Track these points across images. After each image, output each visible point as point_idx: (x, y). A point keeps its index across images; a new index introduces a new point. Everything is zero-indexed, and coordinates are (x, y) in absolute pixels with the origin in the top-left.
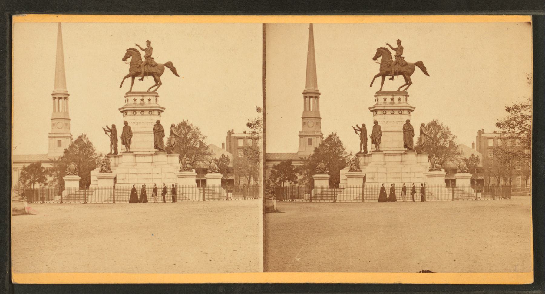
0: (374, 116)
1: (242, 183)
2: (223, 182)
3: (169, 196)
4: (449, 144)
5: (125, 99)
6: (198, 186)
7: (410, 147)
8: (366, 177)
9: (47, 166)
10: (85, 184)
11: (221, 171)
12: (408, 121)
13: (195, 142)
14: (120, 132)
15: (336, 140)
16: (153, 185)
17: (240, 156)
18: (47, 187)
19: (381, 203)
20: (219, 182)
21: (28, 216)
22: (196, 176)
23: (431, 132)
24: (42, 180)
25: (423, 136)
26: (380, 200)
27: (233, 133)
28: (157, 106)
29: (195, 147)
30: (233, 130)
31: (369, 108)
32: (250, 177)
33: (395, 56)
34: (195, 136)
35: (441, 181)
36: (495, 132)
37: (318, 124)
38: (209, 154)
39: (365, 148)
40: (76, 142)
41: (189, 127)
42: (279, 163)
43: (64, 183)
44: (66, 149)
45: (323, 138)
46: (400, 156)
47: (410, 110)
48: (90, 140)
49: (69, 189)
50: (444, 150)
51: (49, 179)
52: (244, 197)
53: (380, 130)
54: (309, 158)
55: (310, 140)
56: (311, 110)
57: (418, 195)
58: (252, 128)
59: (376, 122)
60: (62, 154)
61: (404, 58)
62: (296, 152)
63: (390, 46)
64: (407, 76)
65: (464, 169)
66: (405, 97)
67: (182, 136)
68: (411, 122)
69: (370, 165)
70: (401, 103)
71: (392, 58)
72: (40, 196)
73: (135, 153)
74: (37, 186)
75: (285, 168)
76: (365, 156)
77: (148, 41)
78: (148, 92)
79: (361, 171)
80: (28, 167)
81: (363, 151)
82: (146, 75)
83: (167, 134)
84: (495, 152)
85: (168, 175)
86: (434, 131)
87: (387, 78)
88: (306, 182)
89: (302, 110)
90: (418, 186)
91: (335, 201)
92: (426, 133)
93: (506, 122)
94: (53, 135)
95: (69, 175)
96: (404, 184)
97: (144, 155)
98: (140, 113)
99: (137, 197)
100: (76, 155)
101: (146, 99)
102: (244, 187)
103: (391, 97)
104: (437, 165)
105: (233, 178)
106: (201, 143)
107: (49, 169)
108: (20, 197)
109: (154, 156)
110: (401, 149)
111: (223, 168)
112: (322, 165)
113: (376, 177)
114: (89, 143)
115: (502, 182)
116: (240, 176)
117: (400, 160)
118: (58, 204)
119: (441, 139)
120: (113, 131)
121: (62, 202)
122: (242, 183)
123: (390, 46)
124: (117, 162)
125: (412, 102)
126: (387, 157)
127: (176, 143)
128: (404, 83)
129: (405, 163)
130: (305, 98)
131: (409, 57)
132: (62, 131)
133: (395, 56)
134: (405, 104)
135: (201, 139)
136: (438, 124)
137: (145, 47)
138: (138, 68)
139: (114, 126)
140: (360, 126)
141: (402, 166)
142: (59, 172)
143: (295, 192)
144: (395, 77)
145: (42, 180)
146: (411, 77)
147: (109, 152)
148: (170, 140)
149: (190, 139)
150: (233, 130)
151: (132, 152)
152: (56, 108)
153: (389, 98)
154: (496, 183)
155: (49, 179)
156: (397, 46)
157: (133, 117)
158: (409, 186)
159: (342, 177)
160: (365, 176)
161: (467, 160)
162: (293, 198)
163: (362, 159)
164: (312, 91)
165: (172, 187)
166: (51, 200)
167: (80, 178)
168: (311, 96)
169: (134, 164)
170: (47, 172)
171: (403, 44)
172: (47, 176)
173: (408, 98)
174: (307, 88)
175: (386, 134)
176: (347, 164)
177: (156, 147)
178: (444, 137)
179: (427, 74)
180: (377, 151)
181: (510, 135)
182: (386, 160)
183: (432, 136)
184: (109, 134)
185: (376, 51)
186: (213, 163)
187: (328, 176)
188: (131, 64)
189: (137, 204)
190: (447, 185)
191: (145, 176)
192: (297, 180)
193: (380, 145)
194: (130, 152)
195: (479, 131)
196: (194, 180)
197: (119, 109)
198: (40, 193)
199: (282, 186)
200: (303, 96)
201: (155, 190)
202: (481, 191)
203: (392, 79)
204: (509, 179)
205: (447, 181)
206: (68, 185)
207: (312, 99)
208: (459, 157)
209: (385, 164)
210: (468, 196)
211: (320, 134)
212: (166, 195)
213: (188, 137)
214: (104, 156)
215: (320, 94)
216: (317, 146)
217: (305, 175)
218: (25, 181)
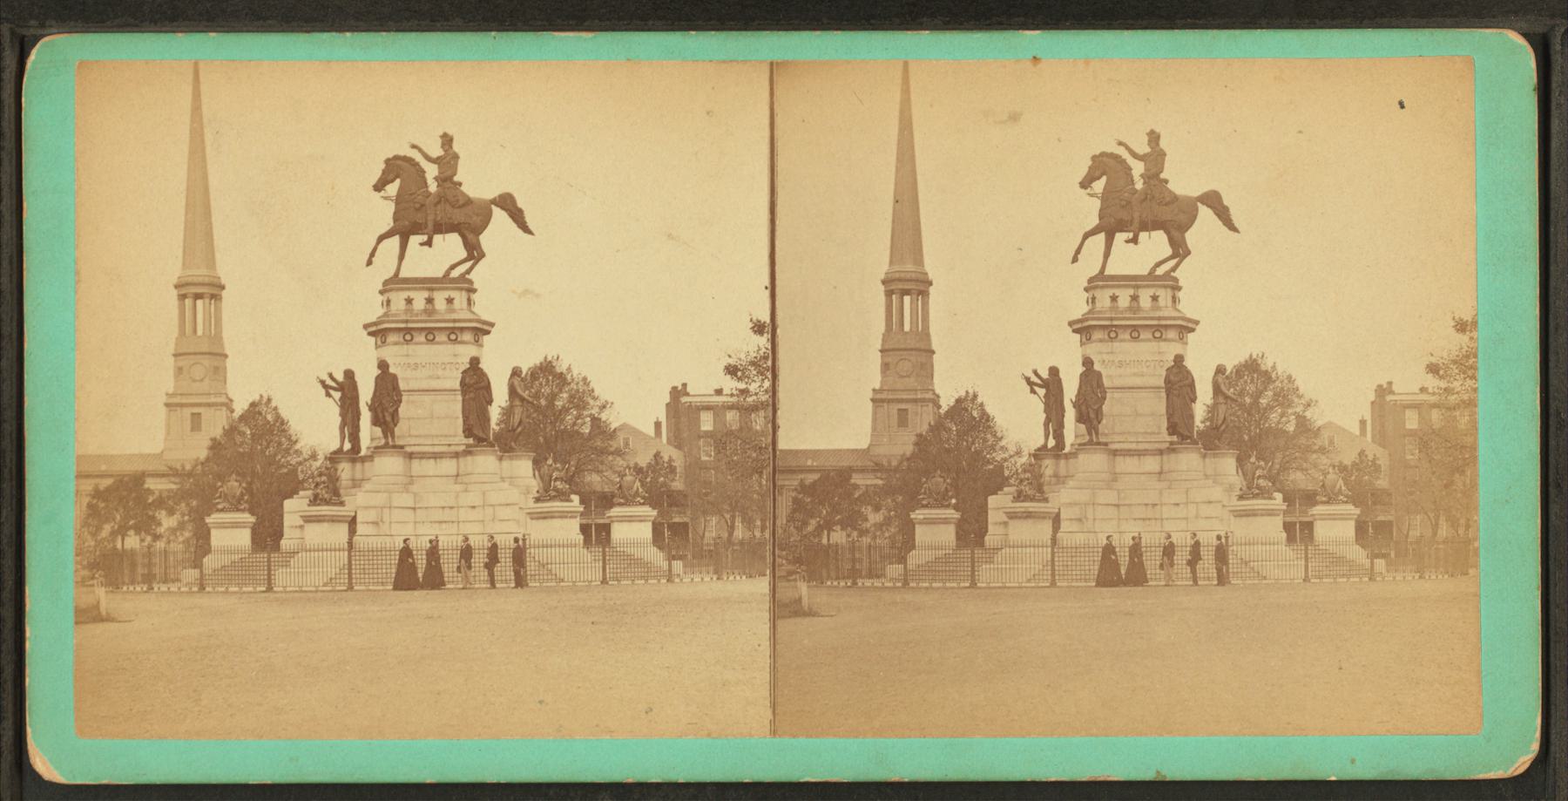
0: (377, 347)
2: (1361, 529)
3: (505, 568)
5: (380, 298)
6: (587, 542)
7: (481, 434)
8: (1063, 516)
9: (160, 487)
11: (1355, 500)
12: (475, 362)
13: (1282, 415)
14: (366, 392)
15: (975, 414)
16: (461, 538)
17: (704, 458)
18: (160, 545)
19: (1104, 589)
20: (645, 531)
22: (582, 514)
23: (1243, 390)
24: (146, 525)
25: (1221, 400)
26: (398, 586)
29: (578, 433)
30: (685, 385)
31: (1070, 324)
32: (733, 517)
33: (436, 178)
34: (580, 400)
35: (1273, 528)
36: (1423, 390)
37: (219, 373)
38: (618, 453)
39: (355, 439)
40: (242, 418)
41: (561, 378)
42: (816, 476)
45: (232, 411)
46: (1158, 458)
47: (481, 330)
48: (284, 413)
49: (223, 551)
50: (1282, 442)
51: (167, 522)
52: (718, 573)
54: (901, 463)
55: (196, 418)
56: (200, 332)
57: (1207, 564)
58: (740, 379)
60: (203, 454)
61: (1166, 181)
62: (158, 451)
64: (1175, 234)
65: (1337, 495)
67: (543, 402)
69: (367, 486)
71: (1132, 182)
72: (140, 570)
73: (408, 449)
74: (132, 542)
75: (831, 488)
76: (353, 461)
78: (1151, 275)
79: (342, 504)
80: (107, 489)
81: (1051, 443)
82: (440, 232)
83: (500, 396)
84: (1424, 445)
85: (504, 513)
86: (1251, 388)
87: (1120, 237)
88: (187, 534)
90: (1208, 539)
91: (270, 589)
92: (525, 395)
93: (1455, 362)
94: (177, 400)
95: (222, 510)
96: (467, 539)
97: (436, 456)
98: (1127, 336)
99: (417, 572)
101: (440, 299)
102: (716, 544)
103: (426, 294)
104: (1262, 482)
106: (595, 420)
108: (86, 573)
109: (1165, 457)
110: (456, 440)
111: (1361, 489)
112: (939, 482)
113: (386, 518)
114: (281, 423)
115: (1444, 531)
116: (705, 513)
117: (1157, 469)
118: (191, 593)
119: (1272, 408)
120: (346, 388)
121: (202, 588)
123: (420, 150)
124: (358, 476)
125: (484, 307)
126: (415, 463)
128: (462, 253)
129: (465, 479)
131: (476, 183)
132: (911, 382)
133: (436, 178)
134: (466, 315)
135: (595, 411)
136: (558, 370)
137: (1143, 148)
139: (1054, 371)
140: (1045, 374)
141: (458, 487)
142: (194, 503)
143: (860, 561)
144: (1143, 236)
145: (146, 525)
146: (1188, 235)
147: (335, 445)
148: (507, 413)
149: (565, 410)
150: (1390, 383)
151: (402, 447)
152: (185, 326)
153: (419, 300)
155: (167, 522)
156: (1148, 150)
158: (1181, 539)
159: (994, 517)
160: (1058, 515)
162: (854, 574)
163: (345, 470)
166: (173, 581)
167: (253, 519)
168: (908, 286)
170: (160, 503)
171: (456, 147)
172: (162, 515)
173: (474, 297)
174: (897, 268)
175: (1116, 395)
177: (468, 432)
178: (1281, 405)
179: (525, 229)
180: (386, 445)
181: (1466, 397)
183: (543, 402)
184: (1042, 392)
186: (629, 478)
188: (399, 200)
189: (416, 593)
190: (1291, 539)
191: (438, 515)
192: (161, 530)
194: (1099, 444)
196: (1278, 522)
197: (366, 327)
198: (140, 560)
199: (825, 541)
200: (175, 292)
201: (466, 553)
202: (1384, 556)
203: (1135, 240)
204: (1462, 521)
205: (1288, 527)
206: (218, 538)
208: (620, 462)
209: (1115, 480)
210: (646, 571)
211: (223, 399)
212: (497, 569)
213: (559, 403)
214: (321, 457)
216: (218, 432)
217: (183, 515)
218: (99, 529)
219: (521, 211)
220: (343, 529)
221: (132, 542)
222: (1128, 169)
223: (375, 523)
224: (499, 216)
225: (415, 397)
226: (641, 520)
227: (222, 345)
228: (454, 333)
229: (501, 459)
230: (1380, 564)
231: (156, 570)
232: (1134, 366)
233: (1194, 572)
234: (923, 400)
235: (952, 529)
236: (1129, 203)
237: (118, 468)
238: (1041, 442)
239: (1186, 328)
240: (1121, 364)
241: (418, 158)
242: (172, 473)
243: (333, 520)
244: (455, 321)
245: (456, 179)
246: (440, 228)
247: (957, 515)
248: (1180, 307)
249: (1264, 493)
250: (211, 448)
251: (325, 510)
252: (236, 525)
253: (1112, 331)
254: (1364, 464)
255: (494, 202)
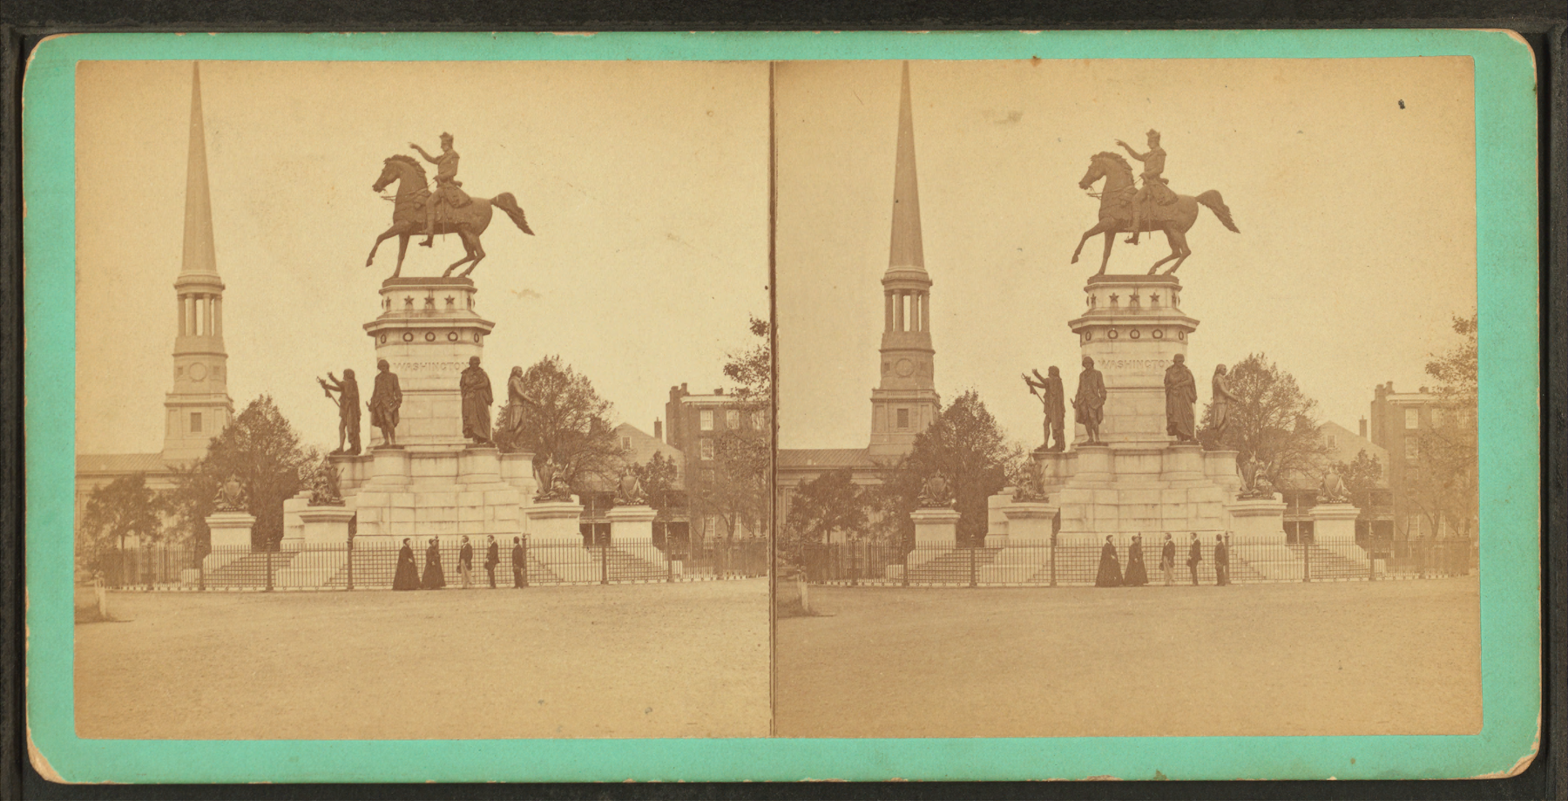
0: (377, 347)
1: (710, 535)
2: (1361, 529)
3: (505, 568)
4: (1293, 422)
5: (380, 298)
6: (587, 542)
7: (481, 434)
8: (1063, 516)
10: (268, 535)
12: (475, 362)
13: (577, 418)
14: (366, 392)
15: (975, 414)
16: (461, 538)
17: (704, 458)
18: (160, 545)
19: (1104, 590)
20: (645, 531)
21: (806, 621)
22: (582, 514)
24: (146, 525)
25: (1221, 399)
26: (398, 586)
27: (1392, 392)
28: (470, 316)
29: (578, 433)
30: (685, 385)
31: (1071, 324)
32: (733, 517)
33: (436, 179)
34: (580, 400)
36: (1423, 390)
37: (219, 373)
40: (242, 418)
42: (816, 476)
43: (209, 533)
44: (214, 440)
45: (232, 411)
47: (481, 330)
48: (284, 413)
51: (167, 522)
53: (396, 387)
55: (196, 418)
56: (200, 332)
57: (1208, 564)
58: (740, 379)
59: (1088, 362)
61: (1166, 181)
62: (865, 446)
63: (420, 150)
64: (1176, 234)
66: (464, 293)
67: (543, 402)
68: (1189, 363)
69: (367, 486)
70: (454, 311)
72: (140, 570)
73: (408, 449)
74: (132, 542)
75: (830, 488)
76: (353, 461)
77: (445, 136)
78: (1151, 275)
79: (342, 504)
80: (108, 489)
81: (1051, 443)
82: (441, 232)
83: (500, 396)
84: (1424, 445)
87: (1120, 237)
88: (187, 534)
89: (882, 327)
90: (1208, 539)
91: (270, 589)
92: (525, 394)
93: (1455, 362)
94: (177, 400)
95: (222, 510)
96: (467, 539)
97: (436, 456)
99: (417, 572)
100: (243, 454)
101: (440, 299)
102: (716, 544)
103: (426, 294)
105: (1390, 518)
106: (595, 420)
107: (165, 494)
108: (86, 573)
110: (456, 440)
111: (1361, 489)
112: (939, 482)
113: (1090, 516)
114: (281, 423)
115: (1444, 530)
116: (705, 513)
117: (1157, 469)
118: (191, 593)
119: (1272, 408)
120: (346, 388)
122: (710, 535)
123: (420, 150)
125: (484, 307)
126: (415, 463)
127: (526, 420)
128: (462, 253)
129: (465, 479)
130: (889, 294)
131: (476, 183)
133: (436, 179)
134: (466, 315)
135: (595, 411)
136: (558, 370)
138: (417, 210)
139: (1054, 371)
140: (1045, 374)
141: (458, 487)
143: (861, 561)
144: (1143, 236)
145: (146, 525)
146: (1188, 235)
147: (335, 445)
148: (507, 412)
149: (565, 410)
150: (1390, 383)
151: (402, 447)
153: (419, 300)
154: (1428, 533)
155: (167, 522)
156: (1147, 150)
157: (1105, 347)
159: (992, 517)
160: (1058, 515)
161: (1345, 468)
162: (854, 574)
163: (345, 470)
164: (908, 276)
165: (513, 545)
166: (878, 577)
167: (253, 519)
168: (908, 286)
169: (406, 480)
170: (160, 503)
171: (456, 147)
172: (162, 515)
173: (474, 297)
175: (1116, 395)
176: (1007, 479)
178: (1281, 405)
180: (386, 445)
181: (1466, 397)
182: (1118, 470)
183: (543, 402)
184: (337, 395)
185: (383, 166)
186: (629, 478)
187: (953, 514)
188: (399, 200)
189: (416, 593)
190: (1291, 539)
191: (438, 515)
192: (161, 530)
193: (1100, 427)
194: (1099, 444)
195: (1380, 386)
196: (575, 524)
197: (366, 327)
198: (139, 560)
199: (825, 541)
200: (175, 293)
201: (466, 553)
202: (1383, 556)
204: (1463, 521)
205: (1288, 527)
206: (218, 538)
207: (907, 299)
210: (646, 571)
211: (223, 399)
213: (559, 403)
214: (321, 457)
215: (931, 284)
216: (218, 433)
217: (183, 515)
218: (99, 529)
219: (521, 211)
220: (343, 529)
221: (132, 542)
222: (1128, 169)
223: (376, 523)
224: (499, 215)
225: (416, 397)
226: (641, 520)
227: (222, 345)
228: (454, 333)
229: (501, 459)
230: (1380, 564)
231: (156, 570)
232: (1134, 366)
233: (1194, 572)
234: (923, 400)
235: (951, 529)
236: (1129, 203)
237: (118, 468)
238: (1041, 442)
239: (1186, 328)
240: (1121, 364)
241: (418, 158)
242: (172, 473)
243: (334, 520)
244: (455, 321)
245: (456, 179)
246: (440, 228)
247: (957, 515)
248: (1180, 307)
249: (1264, 494)
250: (211, 448)
251: (325, 510)
252: (236, 525)
253: (1112, 331)
254: (1363, 464)
255: (494, 202)
